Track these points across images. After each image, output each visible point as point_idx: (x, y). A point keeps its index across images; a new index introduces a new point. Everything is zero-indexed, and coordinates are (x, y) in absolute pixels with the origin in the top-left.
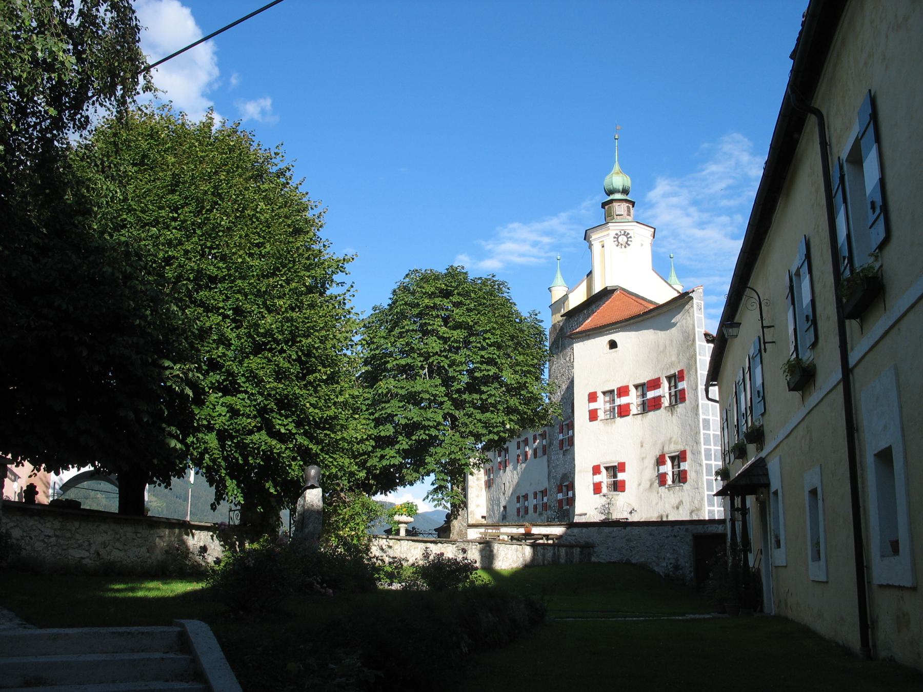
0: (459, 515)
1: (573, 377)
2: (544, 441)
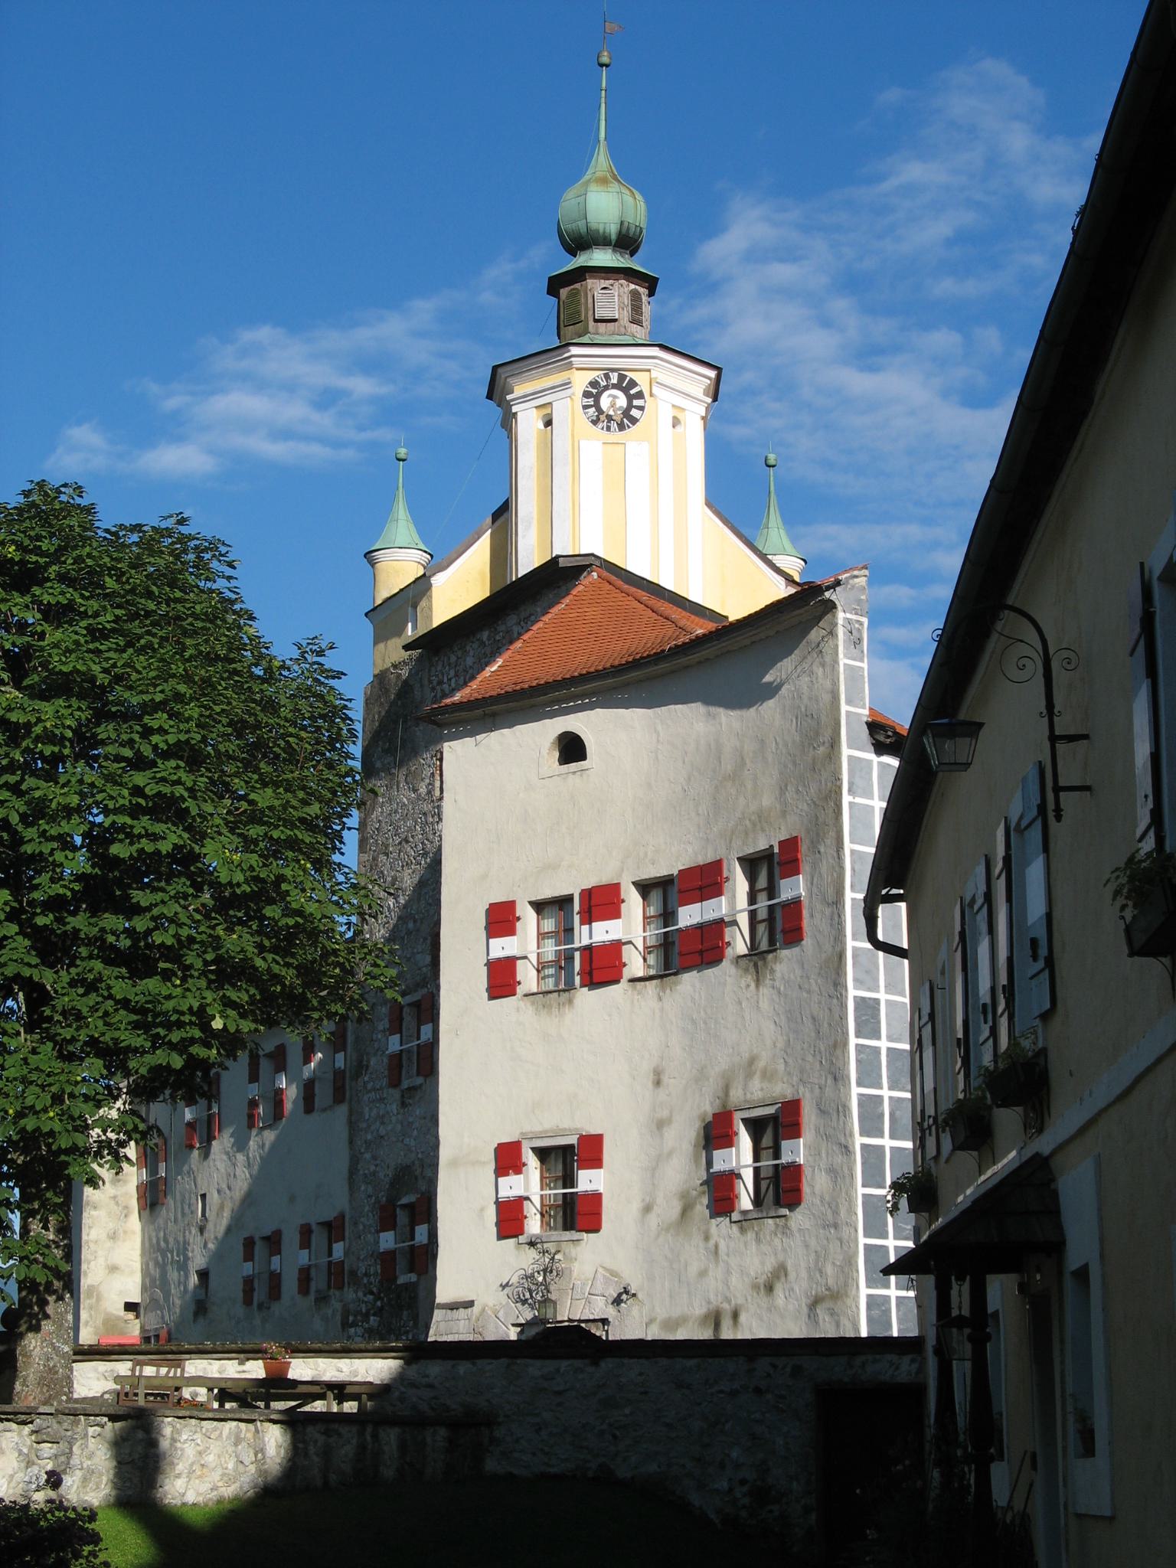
0: (47, 1317)
1: (440, 848)
2: (340, 1056)
